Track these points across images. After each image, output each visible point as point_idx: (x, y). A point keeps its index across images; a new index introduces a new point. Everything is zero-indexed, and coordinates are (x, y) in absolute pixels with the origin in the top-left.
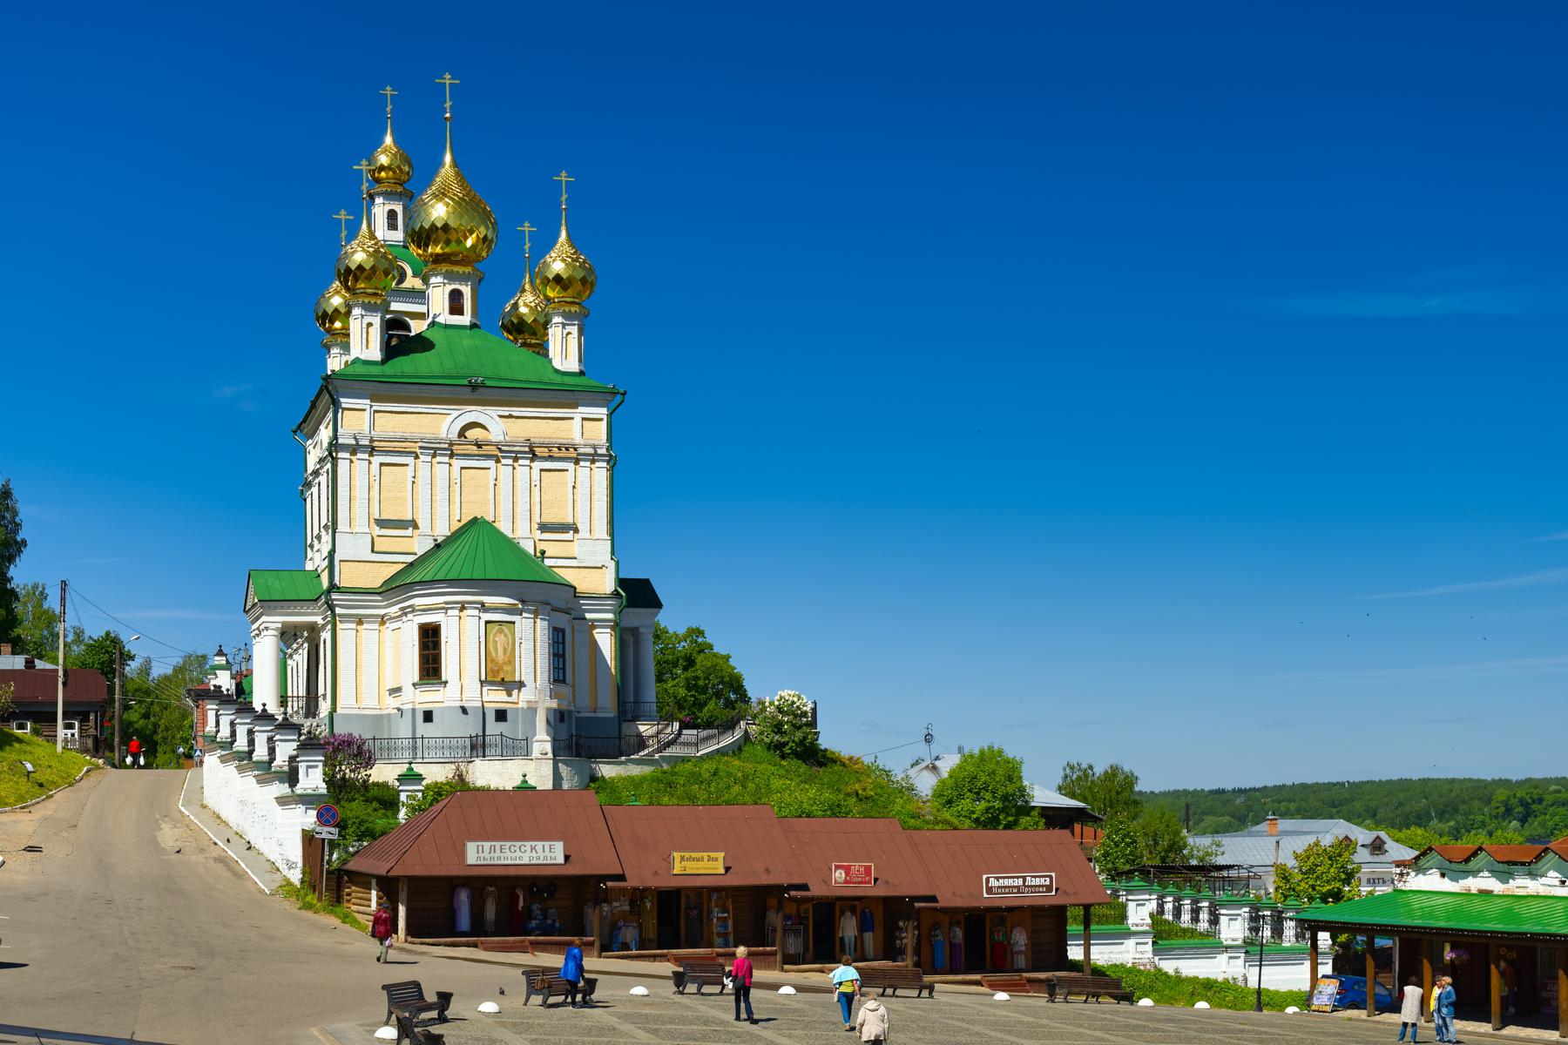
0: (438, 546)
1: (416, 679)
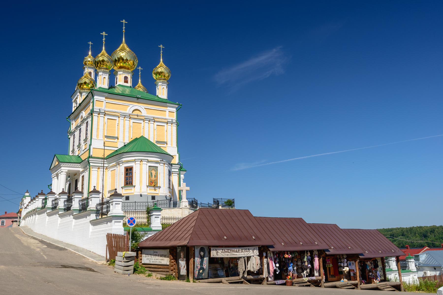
0: (125, 146)
1: (123, 185)
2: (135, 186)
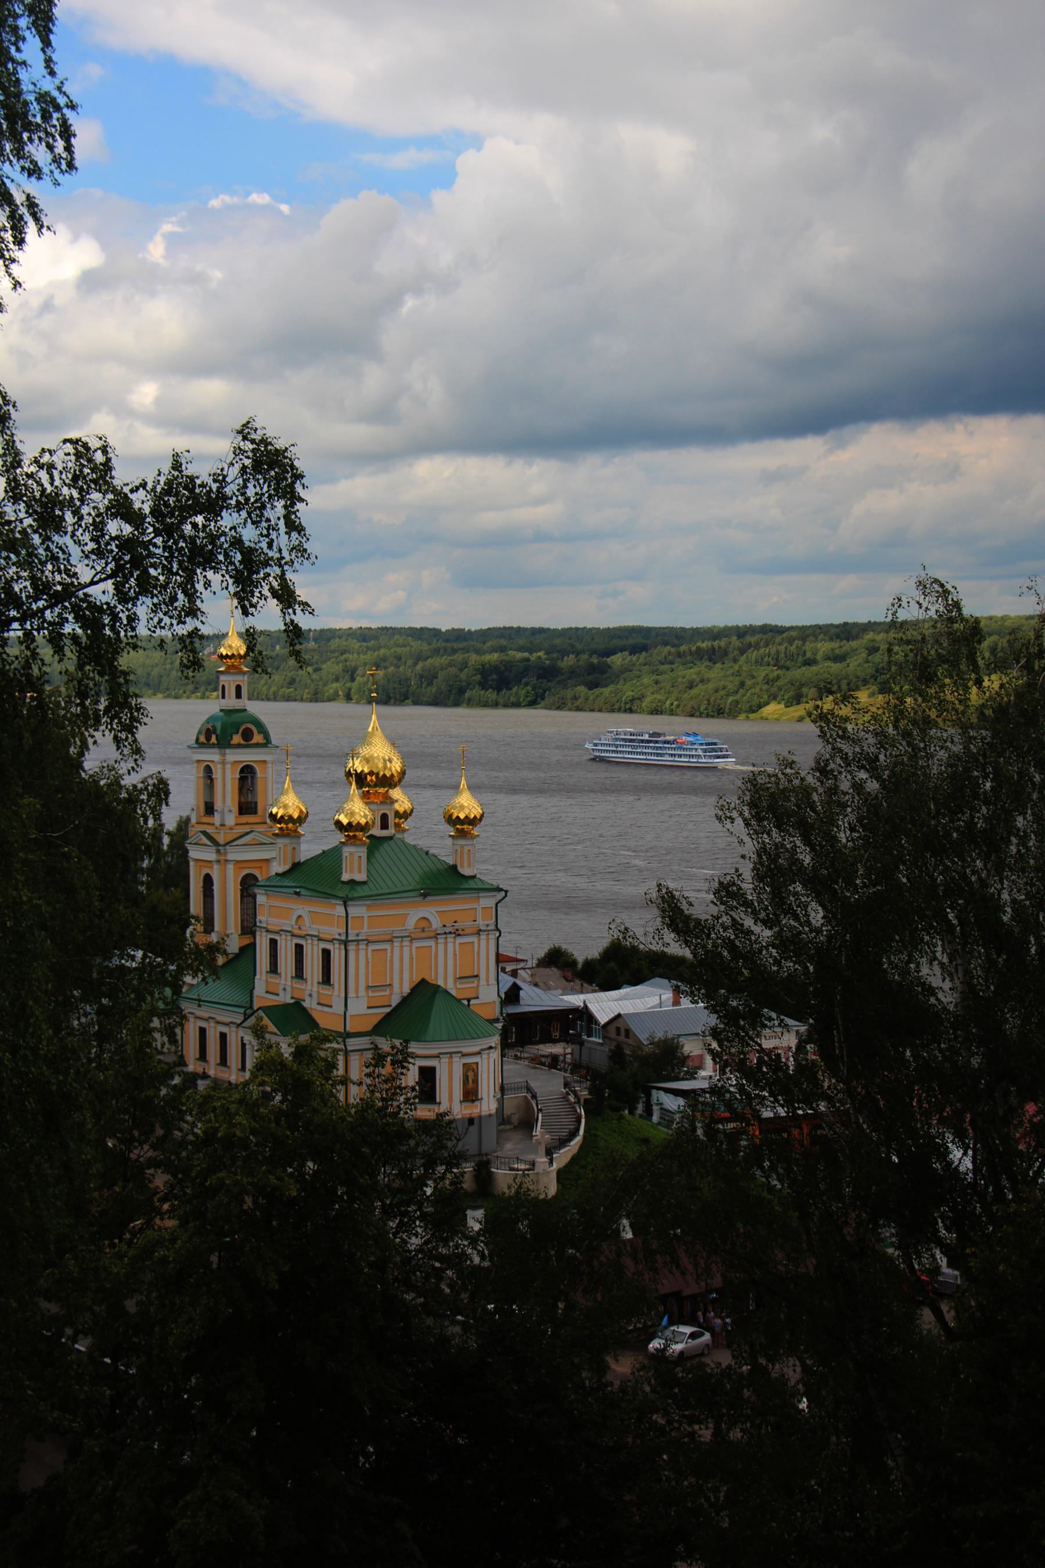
2: (440, 1103)
